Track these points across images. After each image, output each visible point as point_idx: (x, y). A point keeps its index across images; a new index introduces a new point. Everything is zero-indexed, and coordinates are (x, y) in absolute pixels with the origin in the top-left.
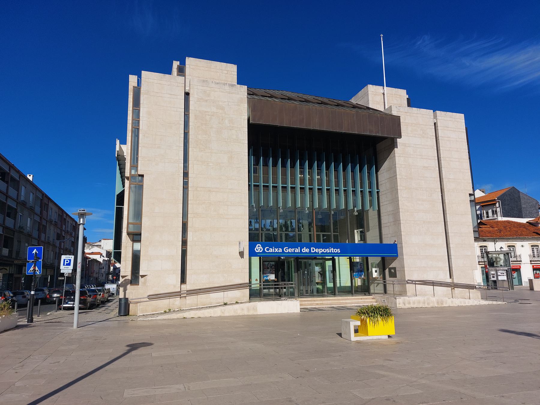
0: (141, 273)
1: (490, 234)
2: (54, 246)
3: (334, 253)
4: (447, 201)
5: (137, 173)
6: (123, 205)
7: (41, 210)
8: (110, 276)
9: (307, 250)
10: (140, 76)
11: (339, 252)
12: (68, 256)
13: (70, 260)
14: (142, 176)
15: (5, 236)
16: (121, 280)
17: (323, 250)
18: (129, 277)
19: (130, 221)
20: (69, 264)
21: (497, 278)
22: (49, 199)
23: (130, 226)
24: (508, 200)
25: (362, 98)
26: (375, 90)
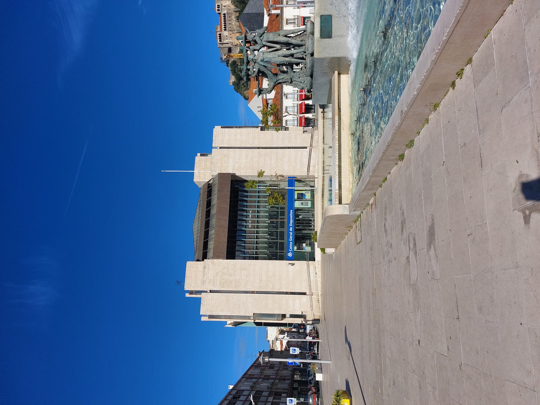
0: (301, 314)
2: (278, 370)
3: (293, 213)
4: (265, 146)
6: (262, 323)
7: (254, 378)
8: (300, 331)
9: (291, 228)
10: (202, 315)
14: (254, 314)
15: (274, 395)
16: (304, 322)
17: (291, 220)
18: (303, 319)
19: (276, 319)
20: (295, 350)
22: (245, 374)
23: (278, 319)
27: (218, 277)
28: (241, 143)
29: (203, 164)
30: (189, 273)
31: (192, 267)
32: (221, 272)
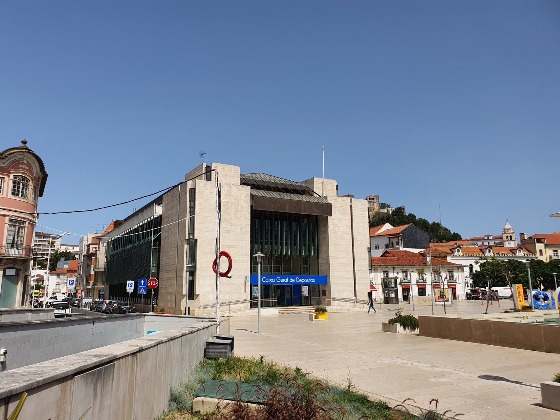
1: (391, 262)
5: (194, 237)
11: (133, 282)
12: (131, 281)
13: (132, 284)
20: (131, 286)
21: (389, 296)
24: (407, 234)
25: (310, 184)
26: (318, 180)
27: (233, 200)
28: (357, 227)
29: (329, 187)
30: (228, 168)
31: (235, 172)
32: (238, 203)
